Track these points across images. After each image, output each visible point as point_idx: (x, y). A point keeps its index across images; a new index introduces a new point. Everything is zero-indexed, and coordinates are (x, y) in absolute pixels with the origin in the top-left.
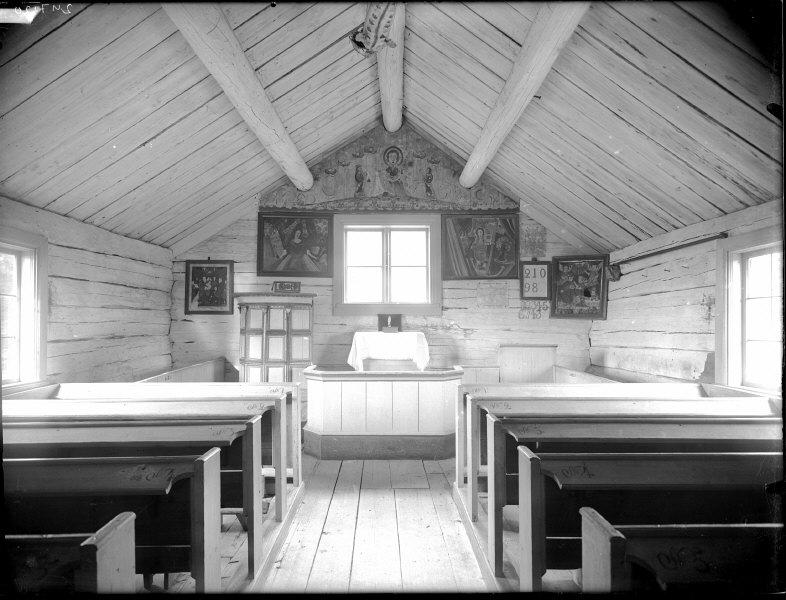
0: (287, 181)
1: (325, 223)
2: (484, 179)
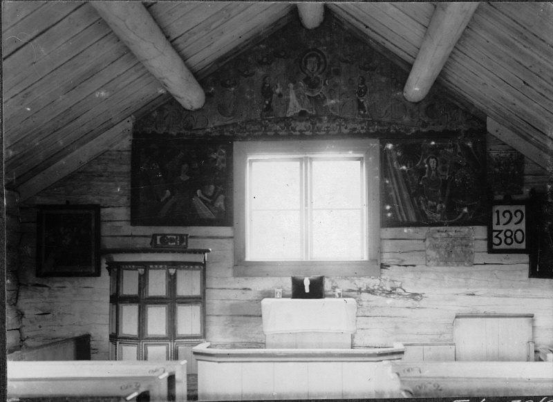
0: (170, 101)
1: (221, 154)
2: (440, 89)
